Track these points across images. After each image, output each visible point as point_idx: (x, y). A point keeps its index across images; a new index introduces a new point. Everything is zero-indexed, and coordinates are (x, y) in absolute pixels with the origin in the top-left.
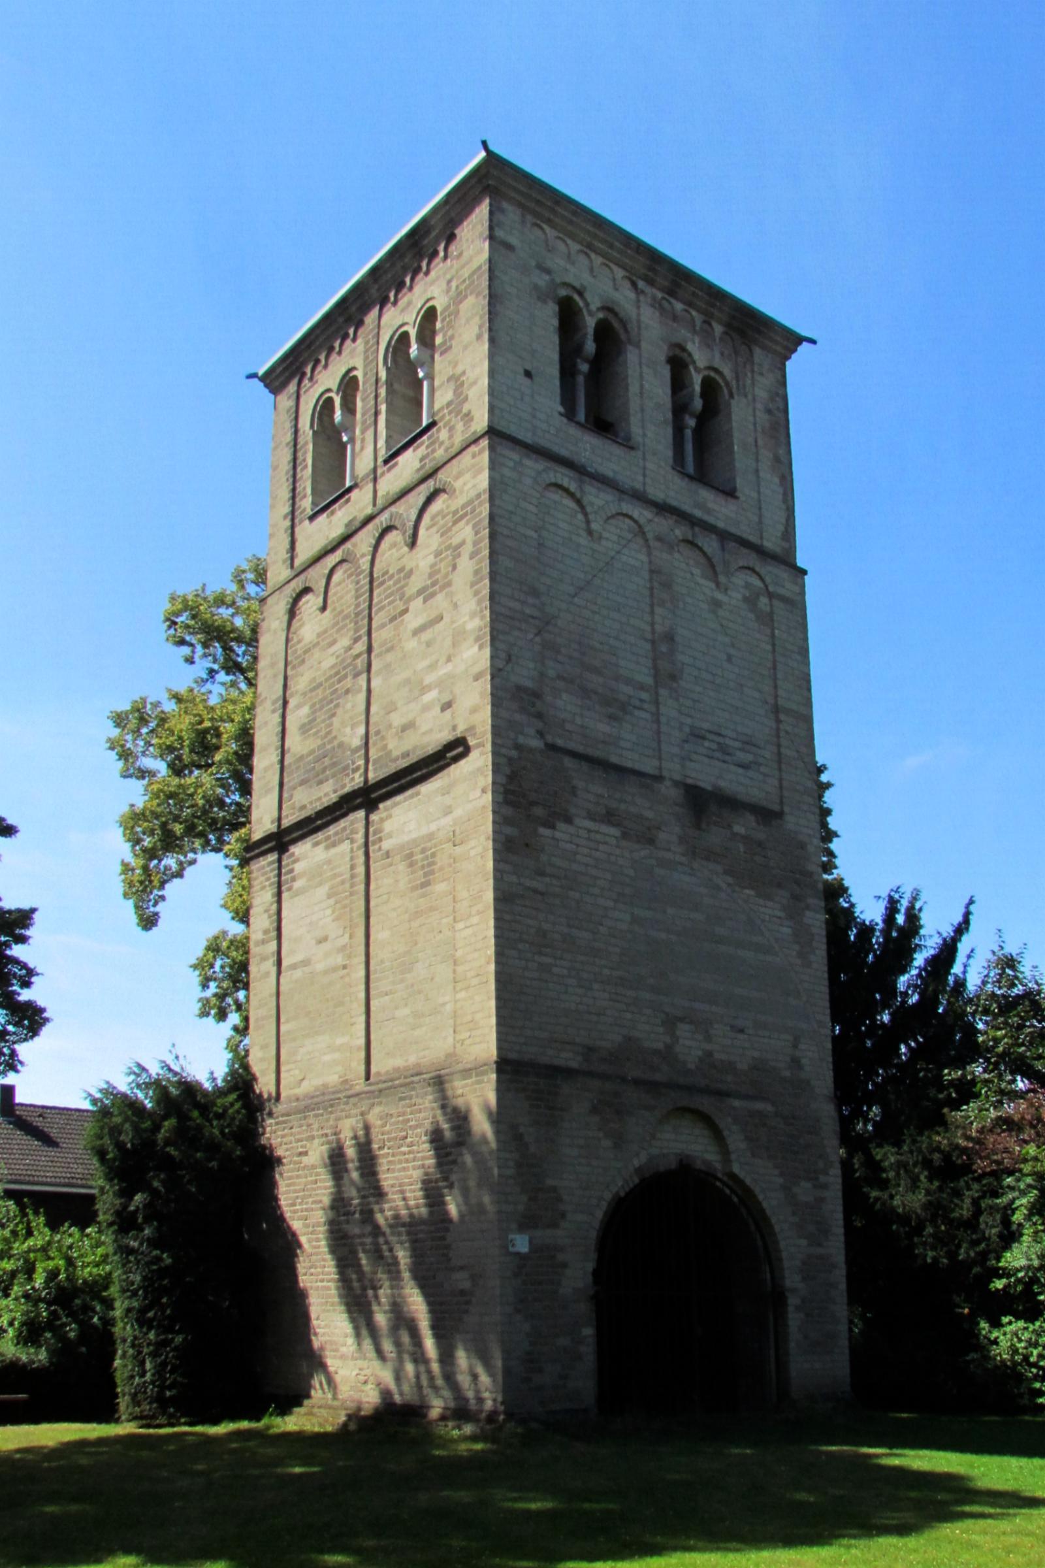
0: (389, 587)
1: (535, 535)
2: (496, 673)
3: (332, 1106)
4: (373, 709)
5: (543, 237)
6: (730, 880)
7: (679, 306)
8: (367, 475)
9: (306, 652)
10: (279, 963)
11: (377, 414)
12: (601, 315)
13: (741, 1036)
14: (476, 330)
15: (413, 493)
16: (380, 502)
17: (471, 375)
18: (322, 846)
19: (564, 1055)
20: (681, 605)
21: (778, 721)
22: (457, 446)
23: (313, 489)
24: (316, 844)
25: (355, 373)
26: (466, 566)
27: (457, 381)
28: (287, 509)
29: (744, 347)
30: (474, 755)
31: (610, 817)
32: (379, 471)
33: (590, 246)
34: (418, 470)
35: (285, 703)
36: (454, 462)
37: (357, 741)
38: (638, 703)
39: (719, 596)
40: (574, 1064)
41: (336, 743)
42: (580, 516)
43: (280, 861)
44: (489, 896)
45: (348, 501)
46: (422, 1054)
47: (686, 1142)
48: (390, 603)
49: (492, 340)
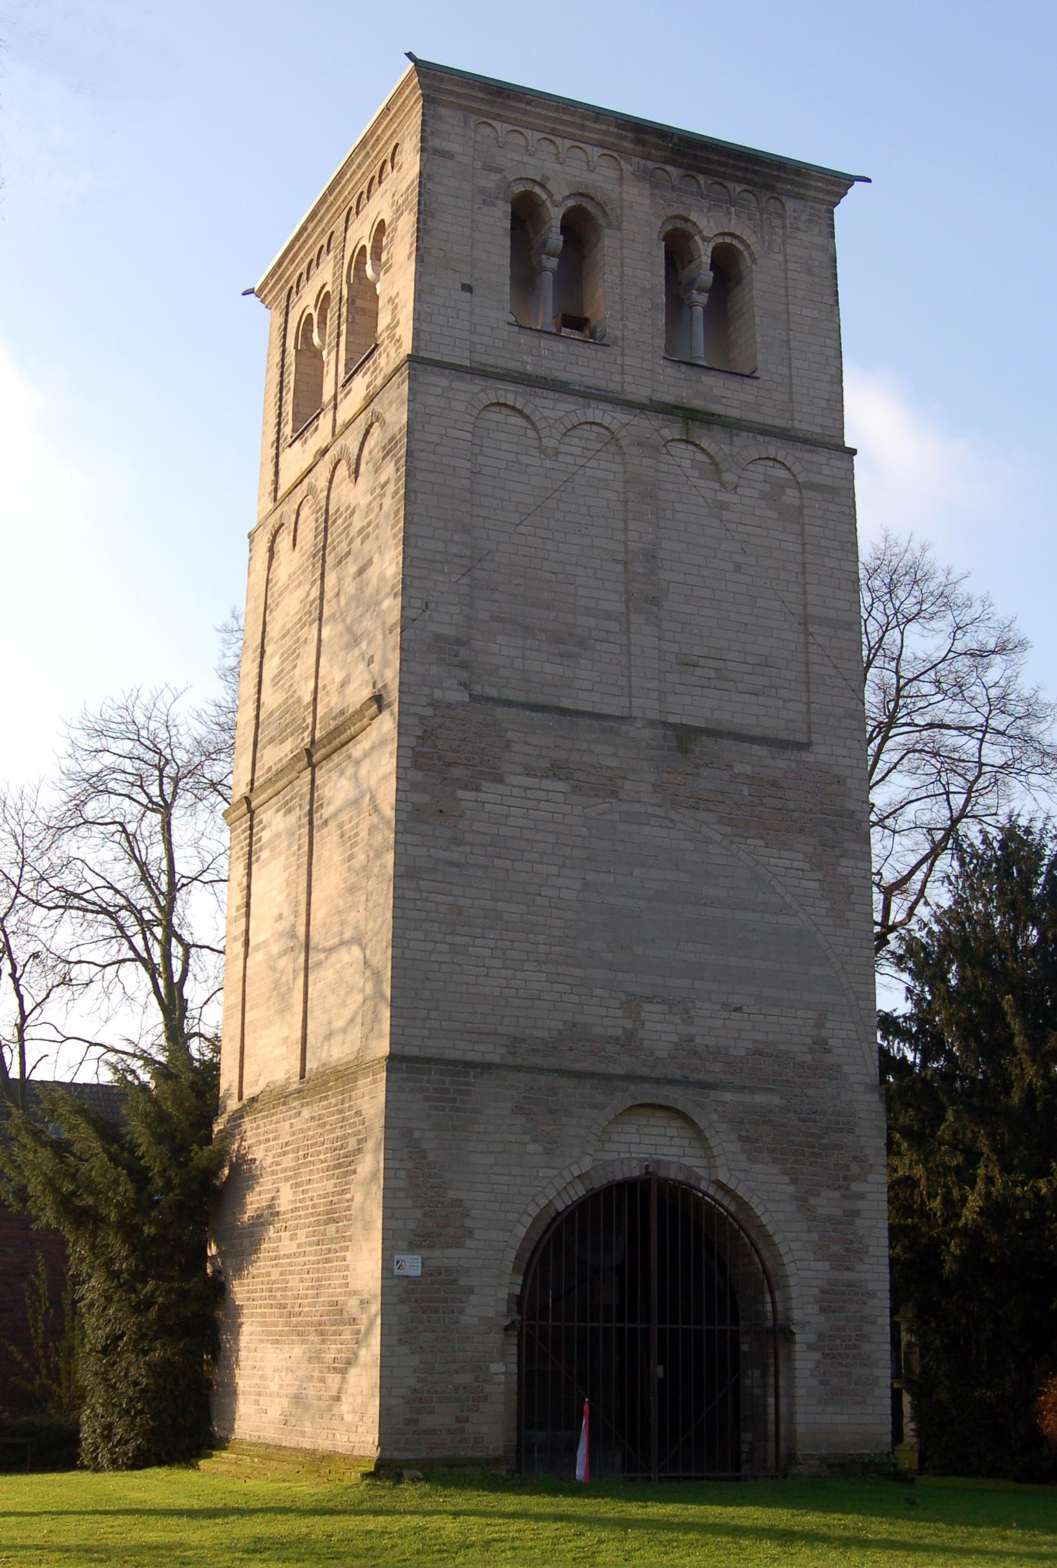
1: (468, 465)
2: (406, 623)
5: (493, 134)
6: (728, 830)
10: (247, 943)
11: (339, 335)
12: (571, 203)
19: (482, 1047)
23: (294, 414)
31: (556, 770)
33: (553, 132)
39: (724, 496)
40: (494, 1058)
42: (531, 433)
47: (647, 1147)
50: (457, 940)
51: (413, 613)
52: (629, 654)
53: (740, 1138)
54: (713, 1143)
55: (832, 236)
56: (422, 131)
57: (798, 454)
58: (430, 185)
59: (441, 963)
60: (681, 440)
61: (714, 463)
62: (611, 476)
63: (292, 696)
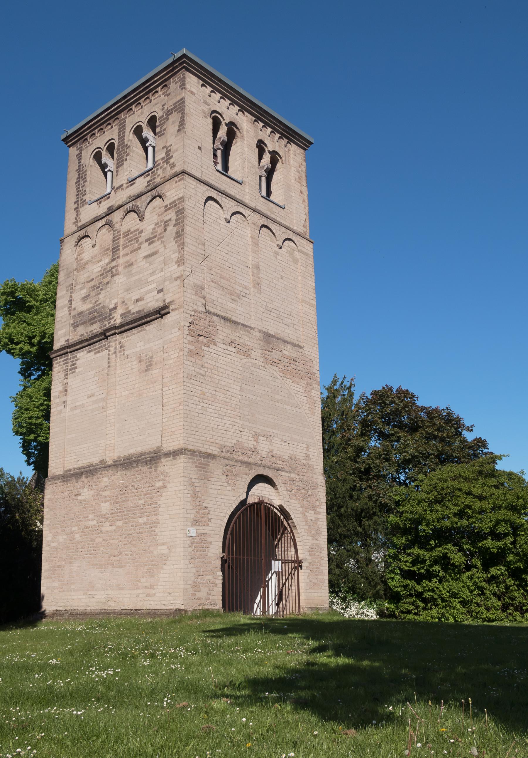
0: (131, 237)
13: (285, 444)
18: (93, 353)
19: (212, 448)
22: (168, 177)
24: (90, 352)
34: (146, 187)
38: (244, 295)
40: (215, 453)
41: (101, 305)
45: (109, 197)
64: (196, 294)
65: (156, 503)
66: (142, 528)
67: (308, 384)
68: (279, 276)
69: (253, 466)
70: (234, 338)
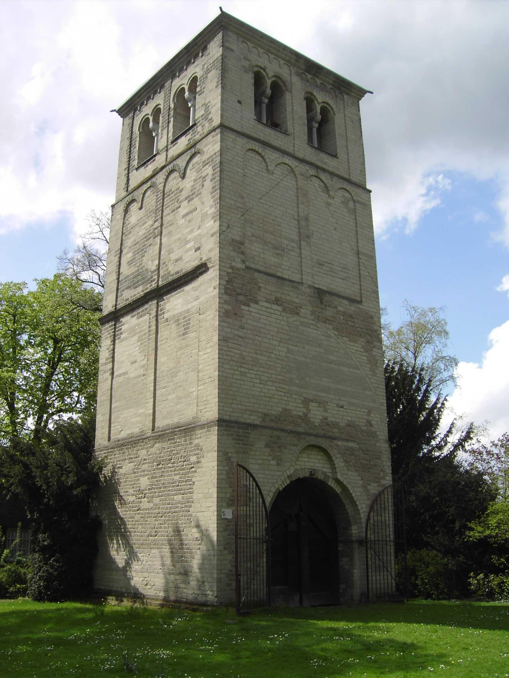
0: (172, 197)
1: (242, 171)
2: (221, 233)
3: (135, 444)
4: (162, 253)
6: (336, 333)
7: (309, 76)
8: (164, 149)
9: (132, 228)
10: (112, 374)
11: (169, 122)
12: (274, 79)
13: (341, 409)
14: (215, 84)
15: (185, 154)
16: (168, 160)
17: (213, 103)
19: (252, 417)
20: (312, 204)
21: (359, 258)
24: (133, 316)
25: (159, 106)
26: (208, 184)
27: (206, 106)
28: (126, 166)
29: (340, 94)
30: (211, 271)
31: (277, 301)
32: (169, 147)
33: (268, 51)
34: (187, 145)
35: (121, 251)
36: (204, 139)
37: (154, 268)
39: (330, 201)
40: (257, 422)
41: (144, 269)
42: (264, 163)
43: (115, 325)
44: (216, 338)
46: (180, 417)
47: (312, 464)
48: (172, 204)
49: (223, 88)
50: (243, 370)
51: (224, 229)
52: (301, 258)
53: (344, 461)
54: (336, 462)
55: (359, 111)
56: (223, 39)
57: (354, 189)
58: (226, 60)
59: (237, 379)
60: (315, 176)
61: (326, 187)
62: (291, 185)
63: (141, 269)
64: (234, 250)
65: (191, 480)
66: (177, 507)
67: (368, 342)
68: (333, 228)
69: (303, 436)
70: (279, 295)
